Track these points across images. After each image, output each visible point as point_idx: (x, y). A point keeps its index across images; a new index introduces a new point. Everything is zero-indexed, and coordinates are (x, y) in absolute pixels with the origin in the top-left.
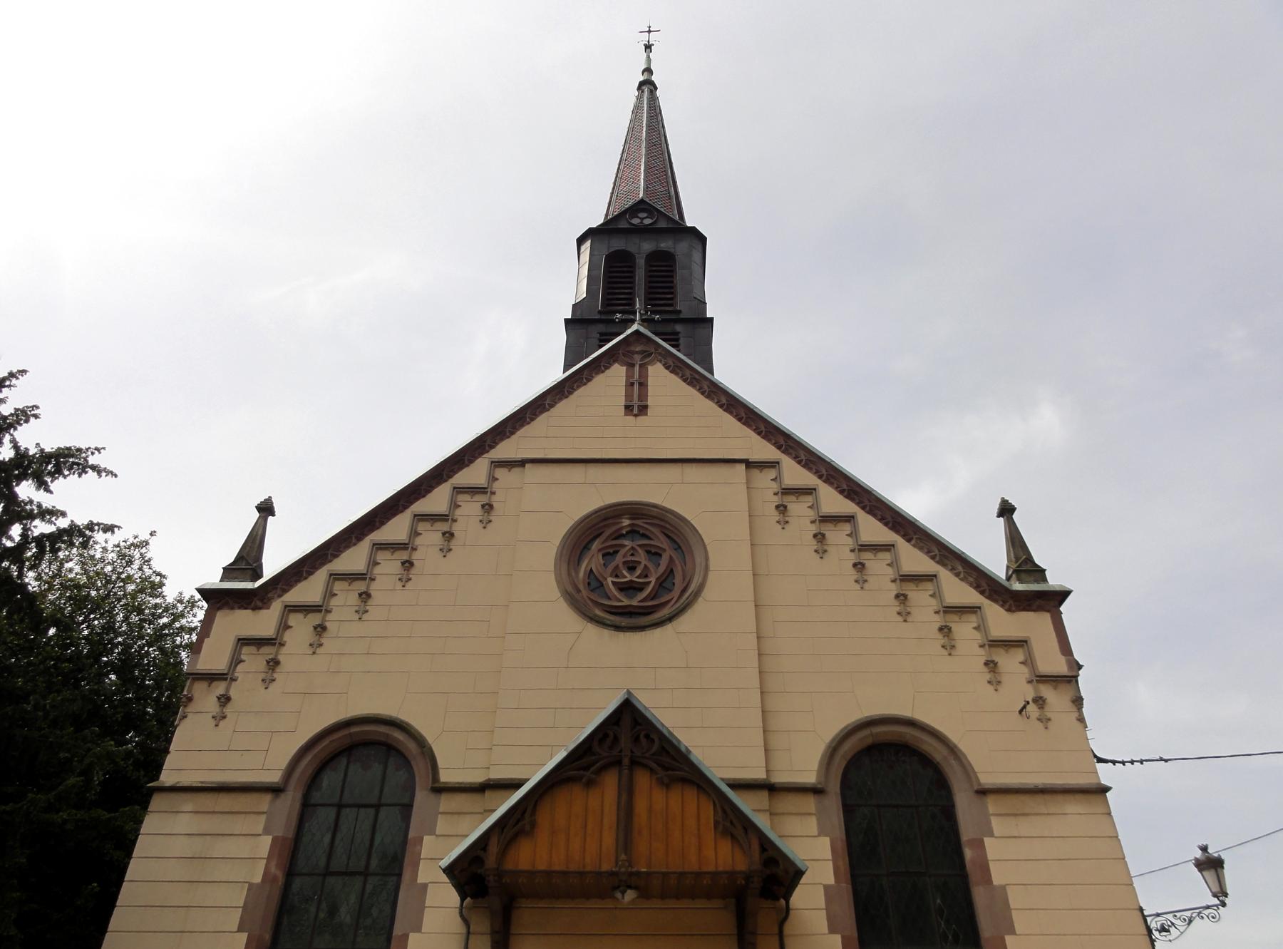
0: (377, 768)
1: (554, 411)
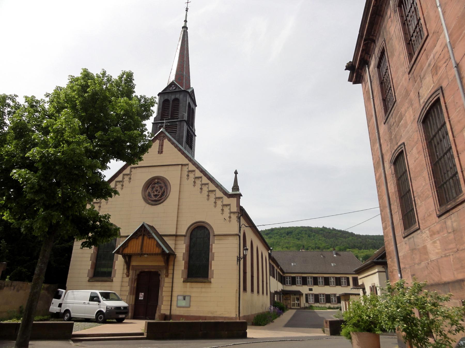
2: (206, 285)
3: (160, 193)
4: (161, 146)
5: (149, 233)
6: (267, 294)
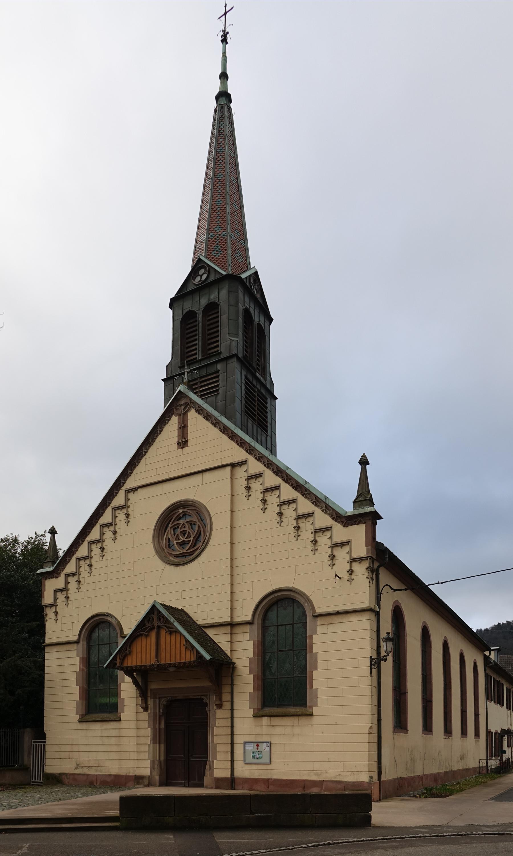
0: (107, 631)
1: (148, 455)
2: (303, 720)
3: (190, 537)
4: (183, 427)
5: (167, 621)
6: (477, 734)
